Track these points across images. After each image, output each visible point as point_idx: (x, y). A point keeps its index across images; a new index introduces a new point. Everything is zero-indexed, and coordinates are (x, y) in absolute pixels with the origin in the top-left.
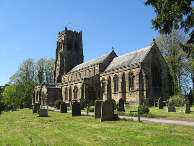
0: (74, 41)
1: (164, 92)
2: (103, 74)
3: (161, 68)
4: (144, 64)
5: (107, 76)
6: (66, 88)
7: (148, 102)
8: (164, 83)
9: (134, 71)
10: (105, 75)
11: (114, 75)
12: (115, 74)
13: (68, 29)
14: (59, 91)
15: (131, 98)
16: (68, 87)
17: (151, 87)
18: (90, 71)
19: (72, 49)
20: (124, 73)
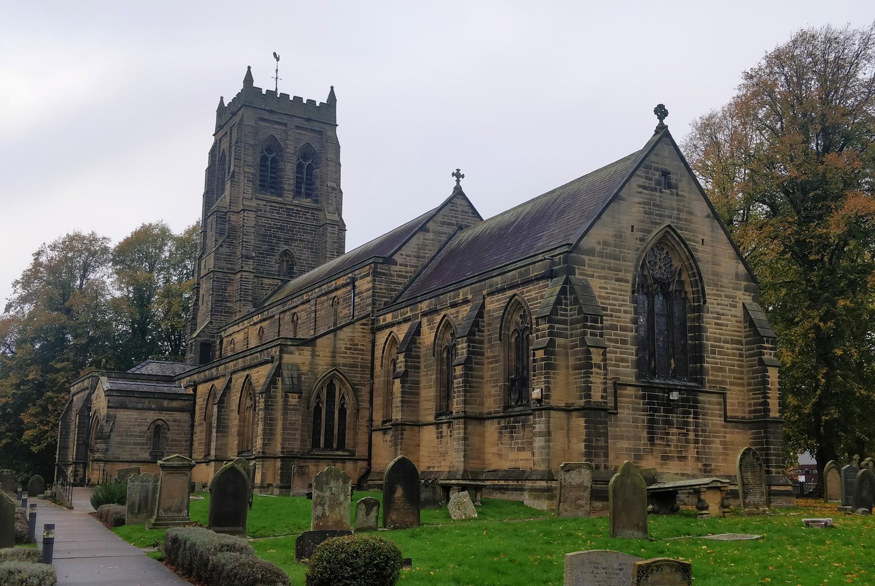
0: (291, 150)
1: (720, 421)
2: (389, 318)
3: (698, 279)
5: (405, 327)
6: (212, 392)
7: (588, 484)
8: (720, 370)
9: (533, 294)
10: (399, 323)
11: (438, 319)
13: (263, 83)
14: (181, 410)
15: (513, 455)
16: (220, 384)
17: (630, 391)
18: (335, 302)
19: (282, 189)
20: (483, 306)
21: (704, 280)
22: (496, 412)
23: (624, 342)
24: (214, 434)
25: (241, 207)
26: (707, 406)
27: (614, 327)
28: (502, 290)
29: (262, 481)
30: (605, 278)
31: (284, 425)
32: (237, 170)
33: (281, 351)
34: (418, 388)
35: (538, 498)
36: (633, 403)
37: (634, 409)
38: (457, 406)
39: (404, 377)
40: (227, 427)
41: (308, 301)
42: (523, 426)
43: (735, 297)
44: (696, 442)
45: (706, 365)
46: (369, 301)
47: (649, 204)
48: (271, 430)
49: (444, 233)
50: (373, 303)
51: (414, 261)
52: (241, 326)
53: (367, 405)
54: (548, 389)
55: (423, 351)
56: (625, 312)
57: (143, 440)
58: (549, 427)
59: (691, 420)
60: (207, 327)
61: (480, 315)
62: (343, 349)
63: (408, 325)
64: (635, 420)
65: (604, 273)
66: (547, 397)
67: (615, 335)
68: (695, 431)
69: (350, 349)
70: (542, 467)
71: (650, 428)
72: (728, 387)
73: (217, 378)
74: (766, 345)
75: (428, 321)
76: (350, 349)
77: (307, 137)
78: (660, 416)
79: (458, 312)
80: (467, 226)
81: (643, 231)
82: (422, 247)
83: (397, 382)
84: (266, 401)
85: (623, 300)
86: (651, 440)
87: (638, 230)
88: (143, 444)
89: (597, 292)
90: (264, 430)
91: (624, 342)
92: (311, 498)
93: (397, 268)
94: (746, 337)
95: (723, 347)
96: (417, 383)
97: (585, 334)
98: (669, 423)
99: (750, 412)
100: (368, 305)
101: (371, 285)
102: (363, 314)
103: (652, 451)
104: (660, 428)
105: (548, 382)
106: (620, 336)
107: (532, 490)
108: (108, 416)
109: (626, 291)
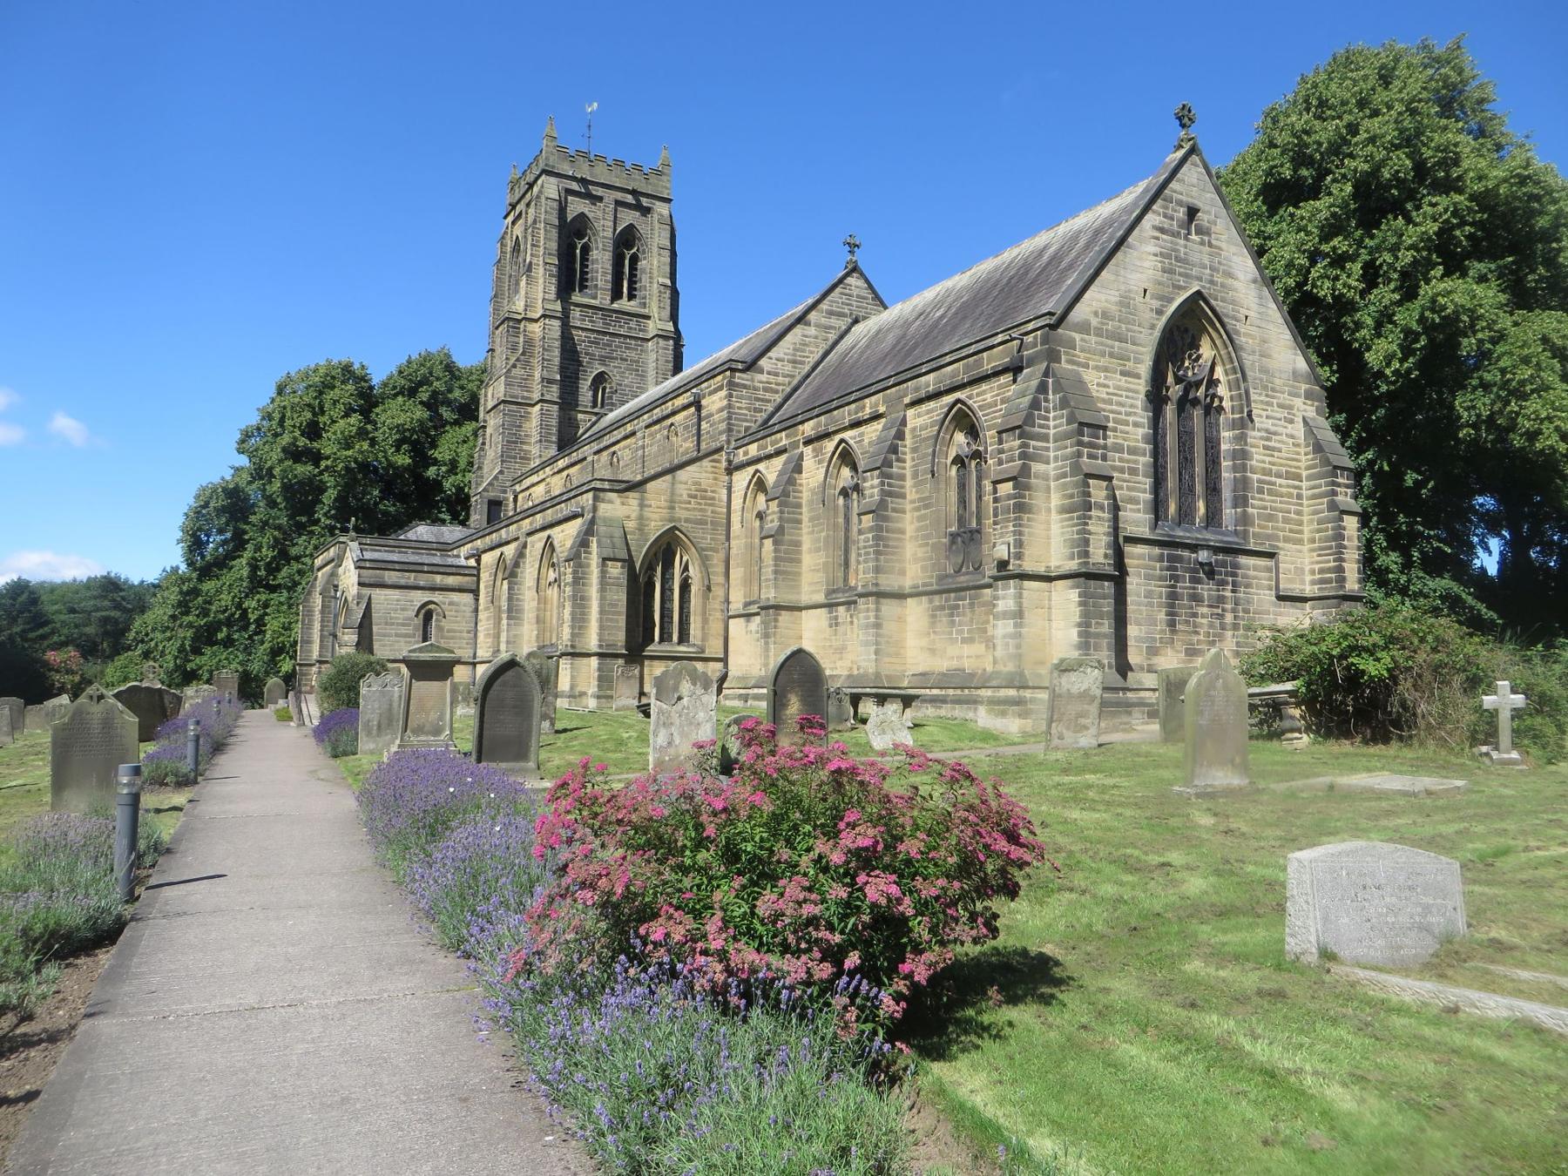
2: (753, 450)
4: (1077, 336)
5: (778, 462)
8: (1270, 518)
10: (769, 457)
12: (837, 438)
15: (953, 650)
16: (510, 551)
20: (904, 422)
21: (1249, 379)
22: (924, 585)
23: (1133, 471)
24: (505, 622)
25: (540, 312)
26: (1251, 573)
27: (1118, 449)
28: (937, 395)
29: (572, 688)
30: (1106, 370)
31: (601, 606)
32: (535, 261)
33: (596, 499)
34: (800, 552)
35: (1003, 714)
36: (1146, 567)
37: (1148, 577)
38: (861, 577)
39: (777, 536)
40: (520, 611)
41: (633, 434)
42: (972, 605)
43: (1290, 407)
44: (1235, 627)
45: (1250, 510)
46: (723, 426)
47: (1169, 257)
48: (583, 614)
49: (831, 327)
50: (729, 430)
51: (788, 368)
52: (541, 475)
53: (721, 579)
54: (1019, 544)
55: (805, 496)
56: (1136, 425)
57: (410, 630)
58: (1020, 605)
59: (1228, 594)
60: (496, 478)
61: (900, 436)
62: (685, 497)
63: (784, 457)
64: (1149, 595)
65: (1103, 362)
66: (1019, 556)
67: (1121, 460)
68: (1234, 611)
69: (695, 497)
70: (1010, 667)
71: (1172, 606)
72: (1281, 544)
73: (508, 543)
74: (1340, 480)
75: (814, 450)
76: (695, 497)
77: (628, 217)
78: (1184, 587)
79: (861, 435)
80: (865, 318)
81: (1161, 298)
82: (800, 347)
83: (768, 543)
84: (575, 572)
85: (1132, 406)
86: (1172, 624)
87: (1154, 297)
88: (406, 636)
89: (1095, 391)
90: (573, 614)
91: (1133, 471)
92: (648, 715)
93: (764, 377)
94: (1308, 468)
95: (1274, 484)
96: (798, 544)
97: (1079, 455)
98: (1196, 598)
99: (1313, 583)
100: (721, 433)
101: (725, 402)
102: (714, 445)
103: (1172, 641)
104: (1183, 606)
105: (1021, 533)
106: (1128, 461)
107: (992, 702)
108: (359, 596)
109: (1136, 392)
